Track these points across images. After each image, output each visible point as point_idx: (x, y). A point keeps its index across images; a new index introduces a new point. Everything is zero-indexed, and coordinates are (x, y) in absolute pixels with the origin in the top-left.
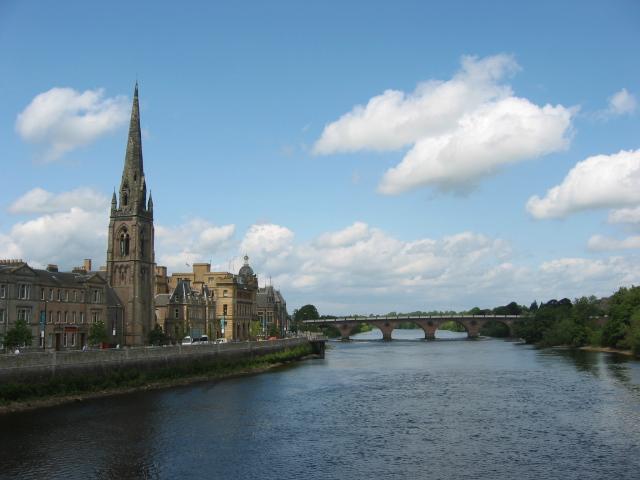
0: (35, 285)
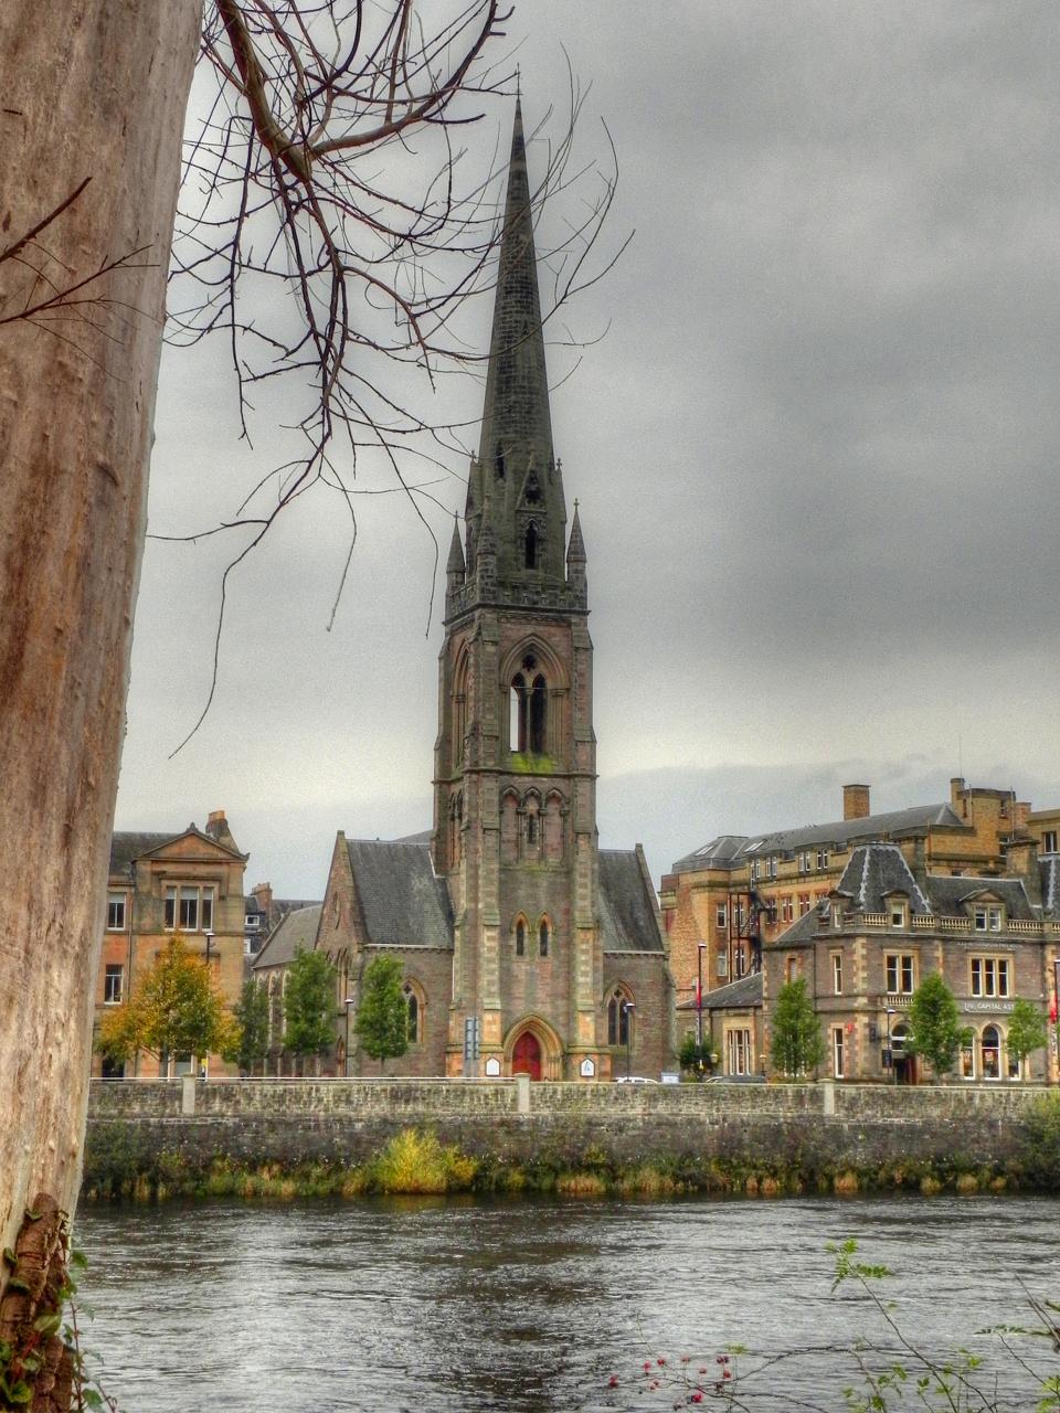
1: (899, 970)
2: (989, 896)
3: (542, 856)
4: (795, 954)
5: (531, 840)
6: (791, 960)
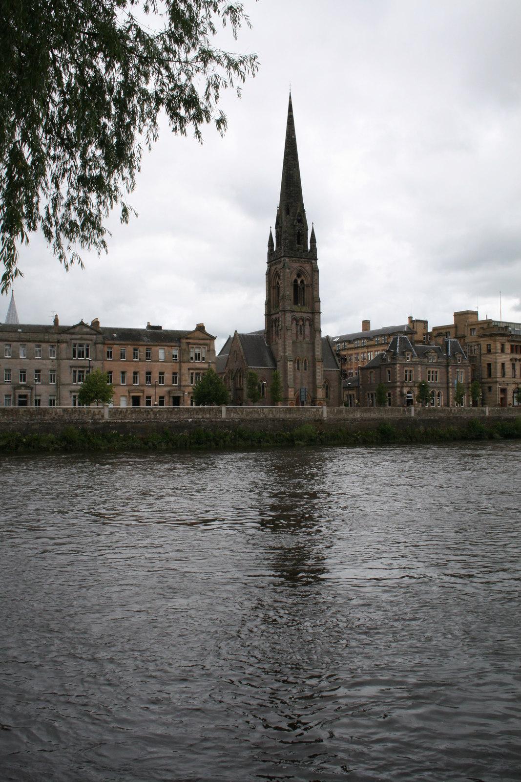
0: (96, 344)
1: (408, 374)
2: (432, 351)
3: (304, 338)
4: (372, 370)
5: (301, 334)
6: (371, 372)
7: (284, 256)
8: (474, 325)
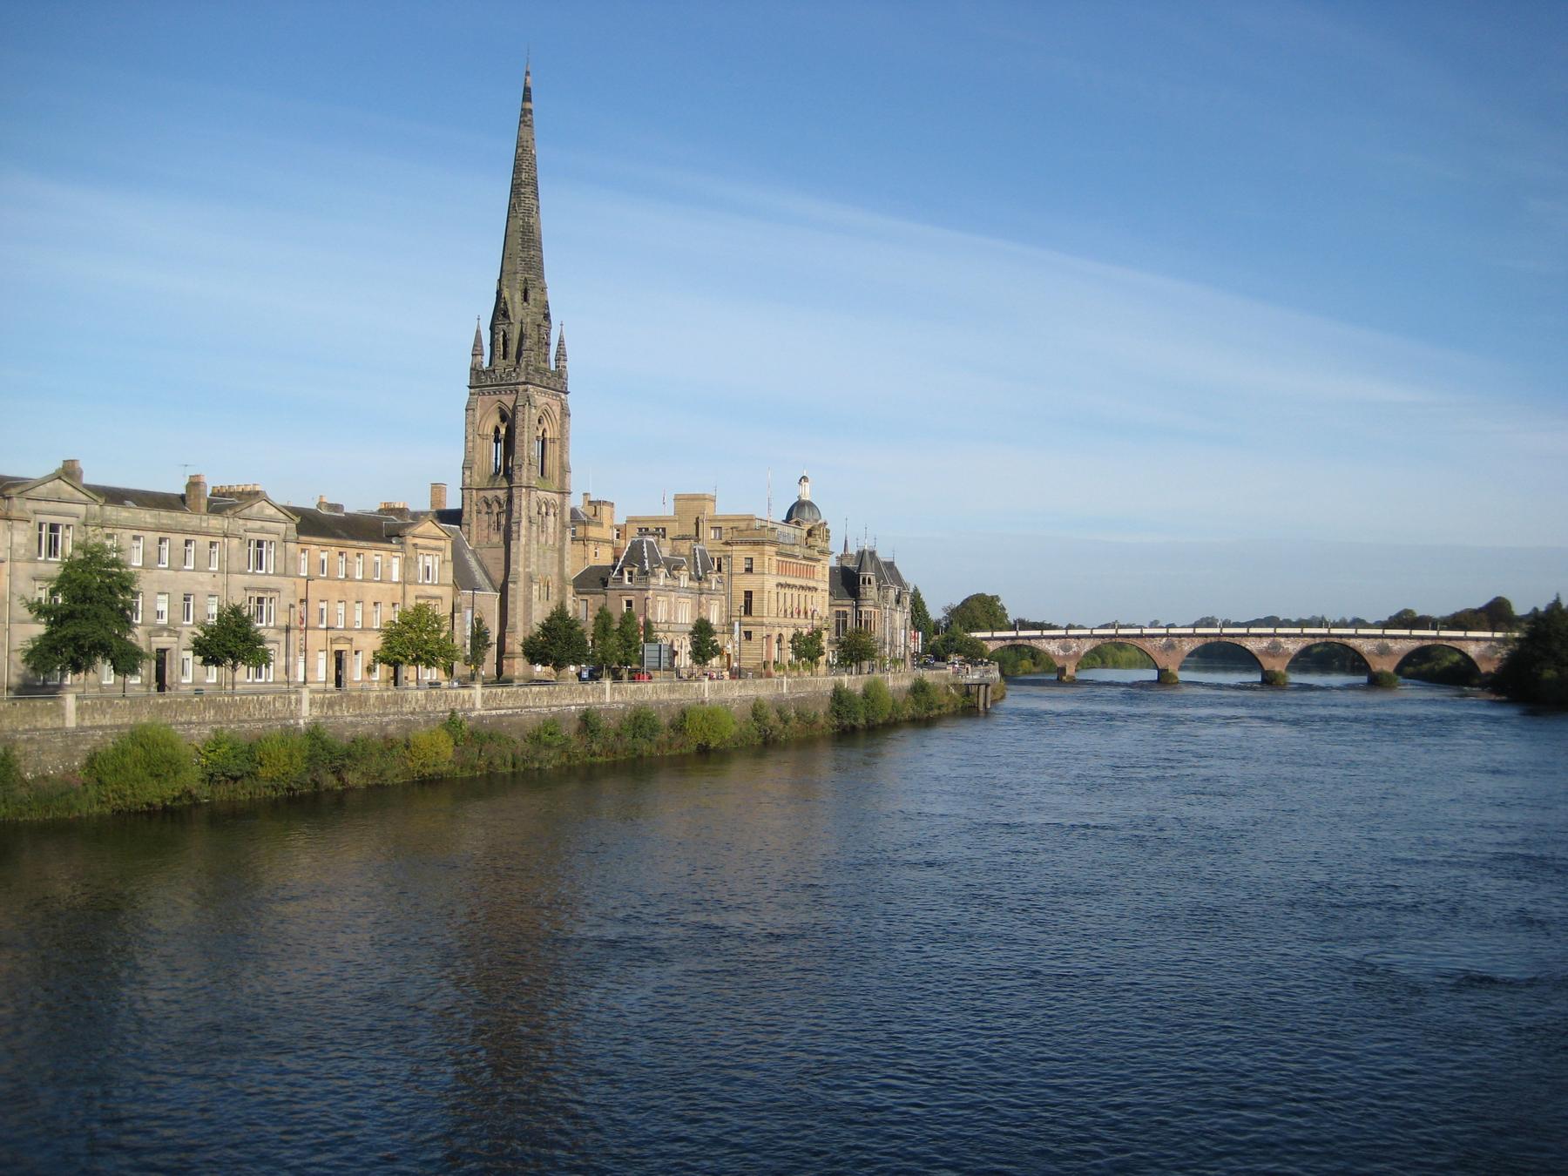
7: (525, 383)
8: (720, 521)
